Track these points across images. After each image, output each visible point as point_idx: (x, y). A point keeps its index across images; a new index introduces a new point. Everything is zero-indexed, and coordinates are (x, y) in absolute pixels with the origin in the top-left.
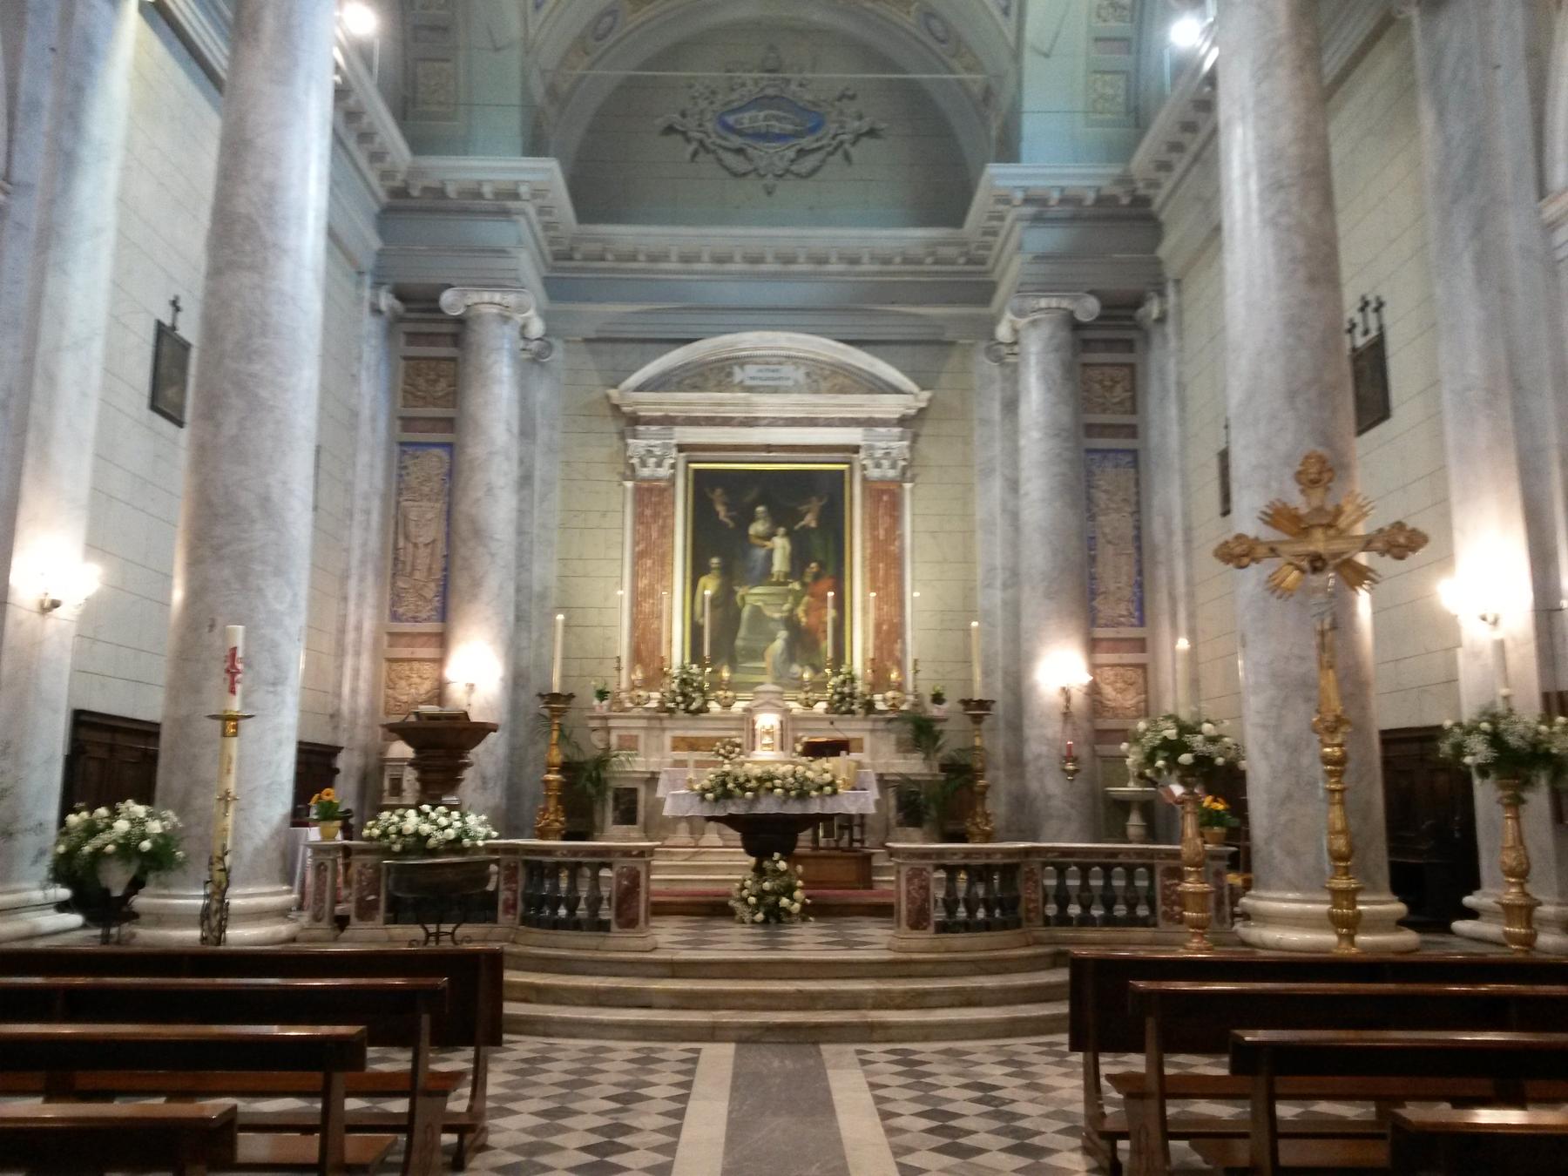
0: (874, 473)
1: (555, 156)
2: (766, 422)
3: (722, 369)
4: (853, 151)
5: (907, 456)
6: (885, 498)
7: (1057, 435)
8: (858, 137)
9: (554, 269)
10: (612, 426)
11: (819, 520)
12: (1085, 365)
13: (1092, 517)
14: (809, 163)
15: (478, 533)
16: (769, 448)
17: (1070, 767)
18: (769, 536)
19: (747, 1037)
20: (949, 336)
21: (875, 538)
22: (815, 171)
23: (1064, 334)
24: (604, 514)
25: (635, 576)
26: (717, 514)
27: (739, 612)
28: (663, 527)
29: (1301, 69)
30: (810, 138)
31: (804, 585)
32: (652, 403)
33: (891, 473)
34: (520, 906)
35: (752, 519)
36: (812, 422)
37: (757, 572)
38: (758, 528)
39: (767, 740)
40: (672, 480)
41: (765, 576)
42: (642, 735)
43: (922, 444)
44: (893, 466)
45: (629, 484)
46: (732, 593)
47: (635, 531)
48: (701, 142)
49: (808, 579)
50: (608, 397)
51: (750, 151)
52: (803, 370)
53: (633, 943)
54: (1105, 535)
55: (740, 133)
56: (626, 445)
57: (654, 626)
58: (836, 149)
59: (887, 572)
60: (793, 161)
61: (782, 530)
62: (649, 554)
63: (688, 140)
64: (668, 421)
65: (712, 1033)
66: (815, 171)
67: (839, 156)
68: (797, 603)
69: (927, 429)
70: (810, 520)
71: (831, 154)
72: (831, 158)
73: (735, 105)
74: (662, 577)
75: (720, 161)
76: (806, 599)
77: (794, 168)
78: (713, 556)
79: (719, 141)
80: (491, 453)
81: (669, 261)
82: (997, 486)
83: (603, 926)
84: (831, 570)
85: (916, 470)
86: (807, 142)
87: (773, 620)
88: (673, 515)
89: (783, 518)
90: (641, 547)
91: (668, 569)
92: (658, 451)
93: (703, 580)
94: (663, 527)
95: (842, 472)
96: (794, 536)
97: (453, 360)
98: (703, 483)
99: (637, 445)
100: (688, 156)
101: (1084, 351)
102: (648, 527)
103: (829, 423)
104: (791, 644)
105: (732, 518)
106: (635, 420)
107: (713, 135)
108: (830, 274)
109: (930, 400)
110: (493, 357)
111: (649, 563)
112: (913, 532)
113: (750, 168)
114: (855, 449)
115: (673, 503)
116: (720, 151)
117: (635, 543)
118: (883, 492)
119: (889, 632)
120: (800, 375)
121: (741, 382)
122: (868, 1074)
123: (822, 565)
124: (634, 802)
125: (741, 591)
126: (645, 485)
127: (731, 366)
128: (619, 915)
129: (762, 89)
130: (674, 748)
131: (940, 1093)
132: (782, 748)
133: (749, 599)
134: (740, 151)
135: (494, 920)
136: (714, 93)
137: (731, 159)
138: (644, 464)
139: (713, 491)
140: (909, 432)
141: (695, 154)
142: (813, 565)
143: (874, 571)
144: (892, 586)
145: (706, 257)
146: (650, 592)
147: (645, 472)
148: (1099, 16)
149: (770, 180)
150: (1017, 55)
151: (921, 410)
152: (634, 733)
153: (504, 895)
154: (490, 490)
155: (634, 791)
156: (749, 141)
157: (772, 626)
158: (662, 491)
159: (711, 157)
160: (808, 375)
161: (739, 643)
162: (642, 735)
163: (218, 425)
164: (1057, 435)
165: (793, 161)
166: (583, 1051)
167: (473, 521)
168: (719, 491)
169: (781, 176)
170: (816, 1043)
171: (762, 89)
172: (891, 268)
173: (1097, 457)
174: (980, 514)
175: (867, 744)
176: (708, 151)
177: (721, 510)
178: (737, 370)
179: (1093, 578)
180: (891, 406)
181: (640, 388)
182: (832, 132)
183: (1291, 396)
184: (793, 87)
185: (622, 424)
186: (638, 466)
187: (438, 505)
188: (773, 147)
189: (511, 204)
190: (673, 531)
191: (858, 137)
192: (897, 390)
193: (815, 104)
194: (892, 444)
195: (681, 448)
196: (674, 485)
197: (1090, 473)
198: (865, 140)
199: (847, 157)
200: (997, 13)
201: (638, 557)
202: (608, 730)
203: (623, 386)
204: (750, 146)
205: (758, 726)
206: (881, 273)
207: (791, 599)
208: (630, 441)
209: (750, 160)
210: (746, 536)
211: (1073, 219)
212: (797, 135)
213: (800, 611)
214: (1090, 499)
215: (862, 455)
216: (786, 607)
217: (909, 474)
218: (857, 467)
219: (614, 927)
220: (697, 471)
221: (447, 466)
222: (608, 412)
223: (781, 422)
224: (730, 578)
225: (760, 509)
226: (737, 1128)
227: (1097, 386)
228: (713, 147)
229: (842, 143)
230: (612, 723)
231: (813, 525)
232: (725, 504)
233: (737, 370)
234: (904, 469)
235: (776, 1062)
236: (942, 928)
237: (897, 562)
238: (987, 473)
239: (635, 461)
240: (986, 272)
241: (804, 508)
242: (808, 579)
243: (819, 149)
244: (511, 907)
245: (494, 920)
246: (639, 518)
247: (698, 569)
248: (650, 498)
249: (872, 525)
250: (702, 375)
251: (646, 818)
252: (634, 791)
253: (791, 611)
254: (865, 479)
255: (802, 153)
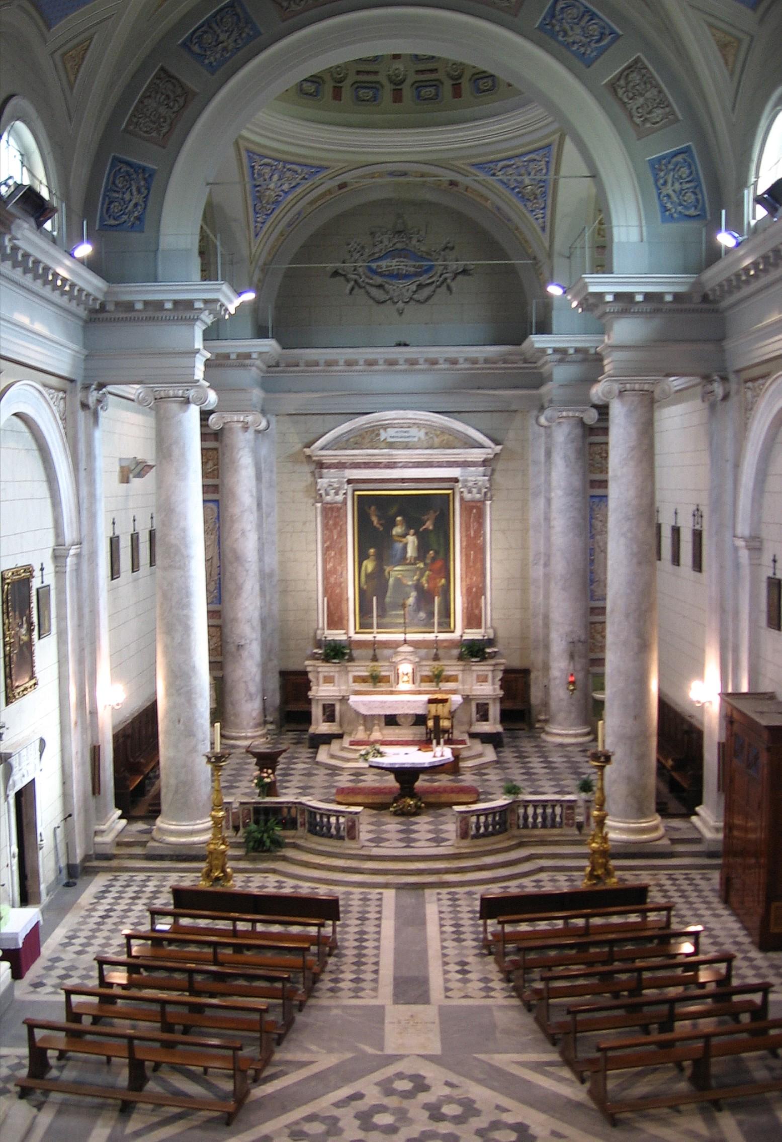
0: (468, 496)
1: (273, 338)
2: (400, 465)
3: (373, 431)
4: (453, 285)
5: (488, 486)
6: (474, 511)
7: (571, 494)
8: (456, 275)
9: (268, 372)
10: (307, 469)
11: (435, 525)
12: (591, 444)
13: (592, 537)
14: (426, 292)
15: (238, 558)
16: (403, 480)
17: (572, 688)
18: (404, 535)
19: (400, 887)
20: (513, 407)
21: (468, 536)
22: (429, 298)
23: (578, 431)
24: (304, 523)
25: (325, 562)
26: (372, 522)
27: (387, 581)
28: (341, 531)
29: (641, 461)
30: (425, 276)
31: (425, 564)
32: (329, 456)
33: (478, 496)
34: (307, 825)
35: (393, 524)
36: (429, 465)
37: (398, 556)
38: (397, 530)
39: (406, 678)
40: (345, 502)
41: (403, 560)
42: (337, 675)
43: (497, 477)
44: (479, 493)
45: (319, 505)
46: (383, 570)
47: (323, 534)
48: (356, 281)
49: (428, 561)
50: (304, 453)
51: (387, 286)
52: (423, 432)
53: (354, 846)
54: (599, 547)
55: (381, 274)
56: (316, 483)
57: (338, 591)
58: (442, 283)
59: (475, 556)
60: (415, 292)
61: (412, 531)
62: (333, 548)
63: (348, 281)
64: (341, 466)
65: (386, 886)
66: (429, 298)
67: (444, 288)
68: (422, 575)
69: (500, 466)
70: (429, 525)
71: (439, 286)
72: (439, 290)
73: (377, 255)
74: (340, 563)
75: (368, 293)
76: (427, 573)
77: (415, 296)
78: (371, 547)
79: (367, 280)
80: (242, 511)
81: (337, 365)
82: (542, 502)
83: (342, 838)
84: (442, 554)
85: (493, 492)
86: (423, 279)
87: (408, 586)
88: (346, 523)
89: (413, 524)
90: (328, 543)
91: (344, 557)
92: (336, 485)
93: (365, 563)
94: (341, 531)
95: (448, 495)
96: (419, 535)
97: (216, 449)
98: (363, 504)
99: (322, 483)
100: (348, 291)
101: (590, 435)
102: (331, 532)
103: (440, 465)
104: (418, 600)
105: (381, 524)
106: (321, 465)
107: (363, 277)
108: (439, 370)
109: (501, 450)
110: (241, 453)
111: (333, 554)
112: (491, 530)
113: (388, 297)
114: (456, 480)
115: (346, 516)
116: (368, 287)
117: (324, 542)
118: (472, 508)
119: (476, 592)
120: (421, 434)
121: (385, 439)
122: (439, 906)
123: (437, 553)
124: (333, 711)
125: (387, 569)
126: (329, 506)
127: (378, 430)
128: (348, 835)
129: (394, 244)
130: (354, 682)
131: (553, 783)
132: (414, 683)
133: (394, 574)
134: (380, 286)
135: (296, 829)
136: (363, 248)
137: (374, 292)
138: (327, 494)
139: (370, 508)
140: (489, 469)
141: (352, 289)
142: (431, 552)
143: (467, 556)
144: (478, 565)
145: (361, 362)
146: (334, 571)
147: (328, 499)
148: (599, 234)
149: (400, 305)
150: (550, 255)
151: (496, 454)
152: (332, 674)
153: (299, 820)
154: (243, 533)
155: (333, 705)
156: (388, 280)
157: (408, 589)
158: (339, 509)
159: (363, 290)
160: (426, 434)
161: (387, 600)
162: (337, 675)
163: (173, 638)
164: (571, 494)
165: (415, 292)
166: (285, 794)
167: (234, 551)
168: (373, 508)
169: (407, 302)
170: (423, 889)
171: (394, 244)
172: (477, 366)
173: (596, 500)
174: (532, 520)
175: (460, 677)
176: (360, 287)
177: (375, 520)
178: (382, 431)
179: (592, 572)
180: (477, 455)
181: (322, 449)
182: (439, 273)
183: (627, 616)
184: (414, 242)
185: (313, 467)
186: (324, 495)
187: (212, 537)
188: (402, 283)
189: (247, 362)
190: (346, 533)
191: (456, 275)
192: (482, 446)
193: (428, 254)
194: (479, 478)
195: (349, 482)
196: (346, 504)
197: (592, 510)
198: (460, 277)
199: (449, 288)
200: (539, 230)
201: (326, 550)
202: (318, 672)
203: (313, 447)
204: (387, 283)
205: (400, 672)
206: (472, 369)
207: (418, 573)
208: (319, 480)
209: (387, 292)
210: (391, 536)
211: (584, 360)
212: (416, 274)
213: (424, 580)
214: (591, 525)
215: (460, 485)
216: (415, 578)
217: (489, 495)
218: (457, 491)
219: (346, 839)
220: (359, 496)
221: (216, 515)
222: (304, 460)
223: (410, 465)
224: (381, 560)
225: (399, 518)
226: (398, 931)
227: (598, 457)
228: (363, 285)
229: (446, 279)
230: (320, 669)
231: (431, 528)
232: (377, 516)
233: (382, 431)
234: (486, 493)
235: (409, 898)
236: (477, 836)
237: (482, 550)
238: (536, 495)
239: (321, 492)
240: (535, 368)
241: (425, 517)
242: (428, 561)
243: (433, 282)
244: (303, 825)
245: (296, 829)
246: (325, 526)
247: (362, 556)
248: (332, 513)
249: (466, 527)
250: (360, 435)
251: (341, 716)
252: (333, 705)
253: (419, 580)
254: (462, 499)
255: (420, 286)
